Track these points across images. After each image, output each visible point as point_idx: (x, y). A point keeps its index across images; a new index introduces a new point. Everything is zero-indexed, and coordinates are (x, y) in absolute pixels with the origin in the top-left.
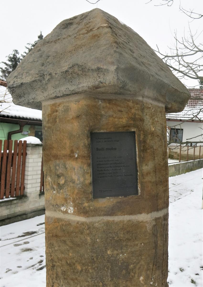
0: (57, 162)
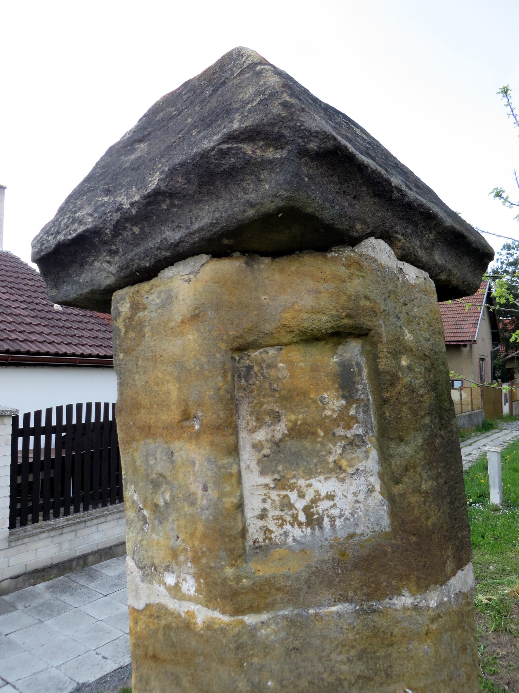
0: (151, 444)
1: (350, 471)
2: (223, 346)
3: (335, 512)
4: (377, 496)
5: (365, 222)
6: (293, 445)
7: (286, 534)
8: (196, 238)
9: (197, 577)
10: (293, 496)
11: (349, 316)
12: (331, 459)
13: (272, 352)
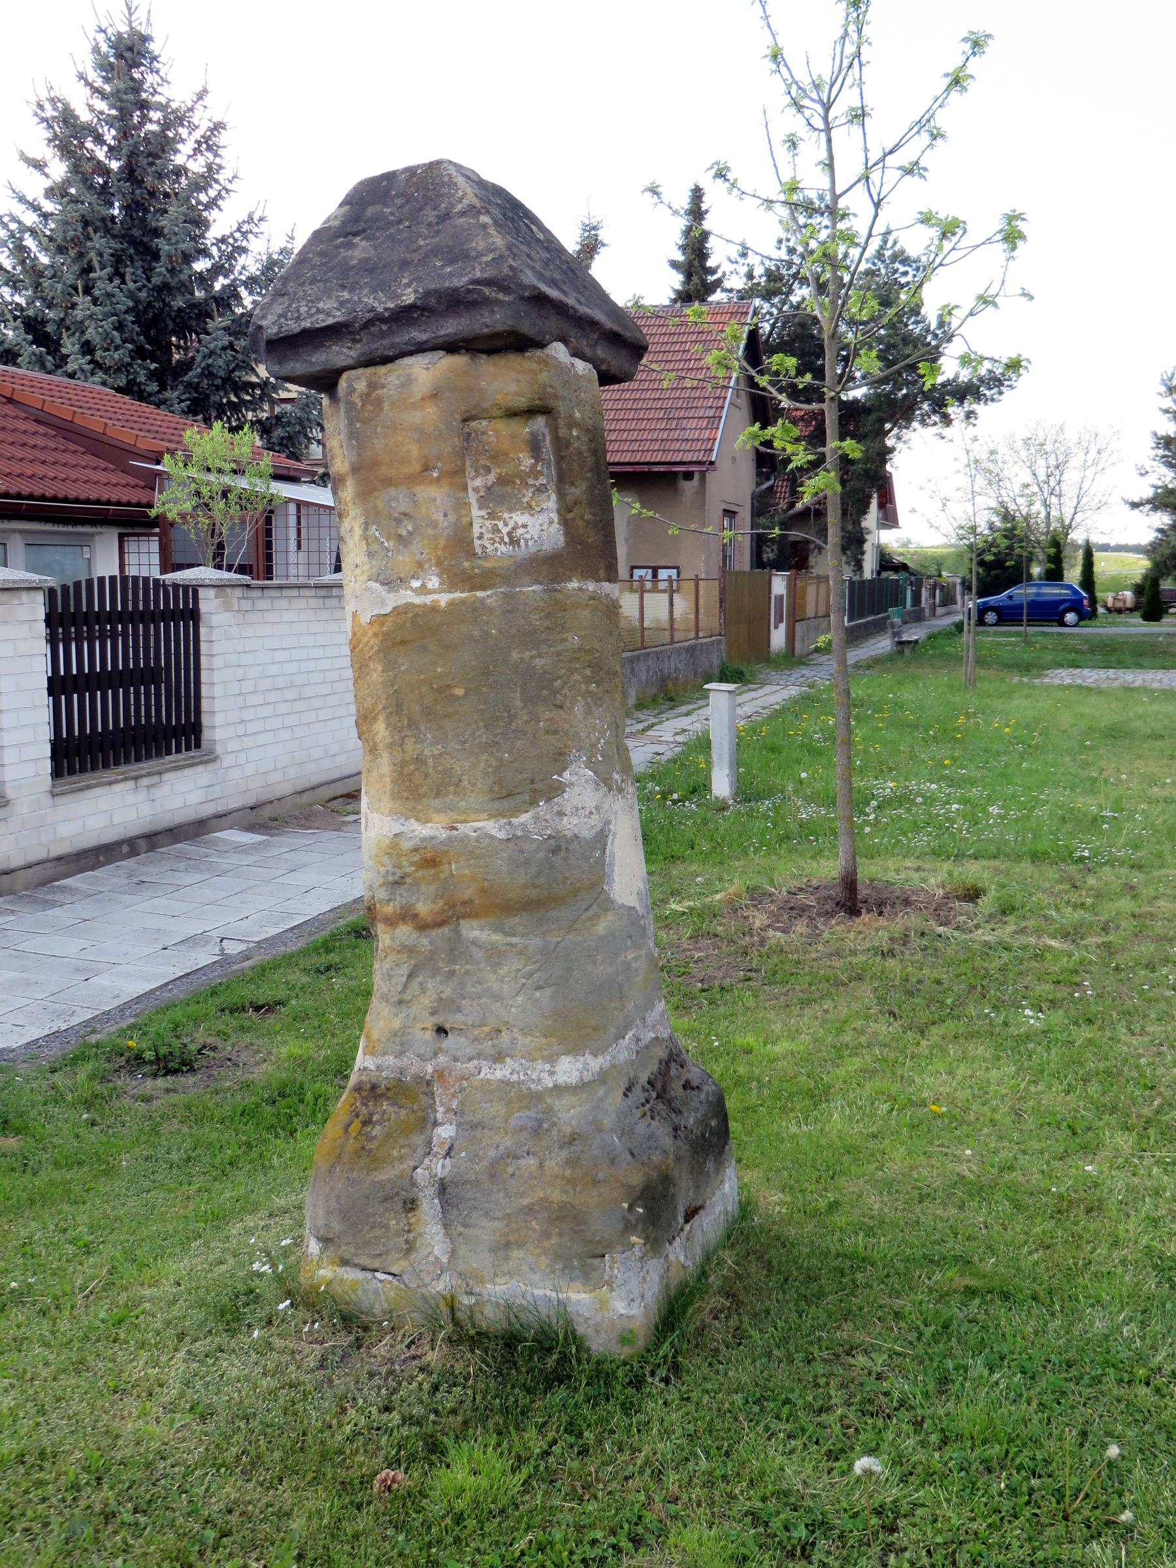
0: (393, 491)
1: (538, 509)
2: (458, 417)
3: (528, 536)
4: (556, 526)
5: (551, 334)
6: (498, 490)
7: (496, 550)
8: (440, 341)
9: (440, 576)
10: (500, 525)
11: (540, 399)
12: (525, 500)
13: (484, 423)
